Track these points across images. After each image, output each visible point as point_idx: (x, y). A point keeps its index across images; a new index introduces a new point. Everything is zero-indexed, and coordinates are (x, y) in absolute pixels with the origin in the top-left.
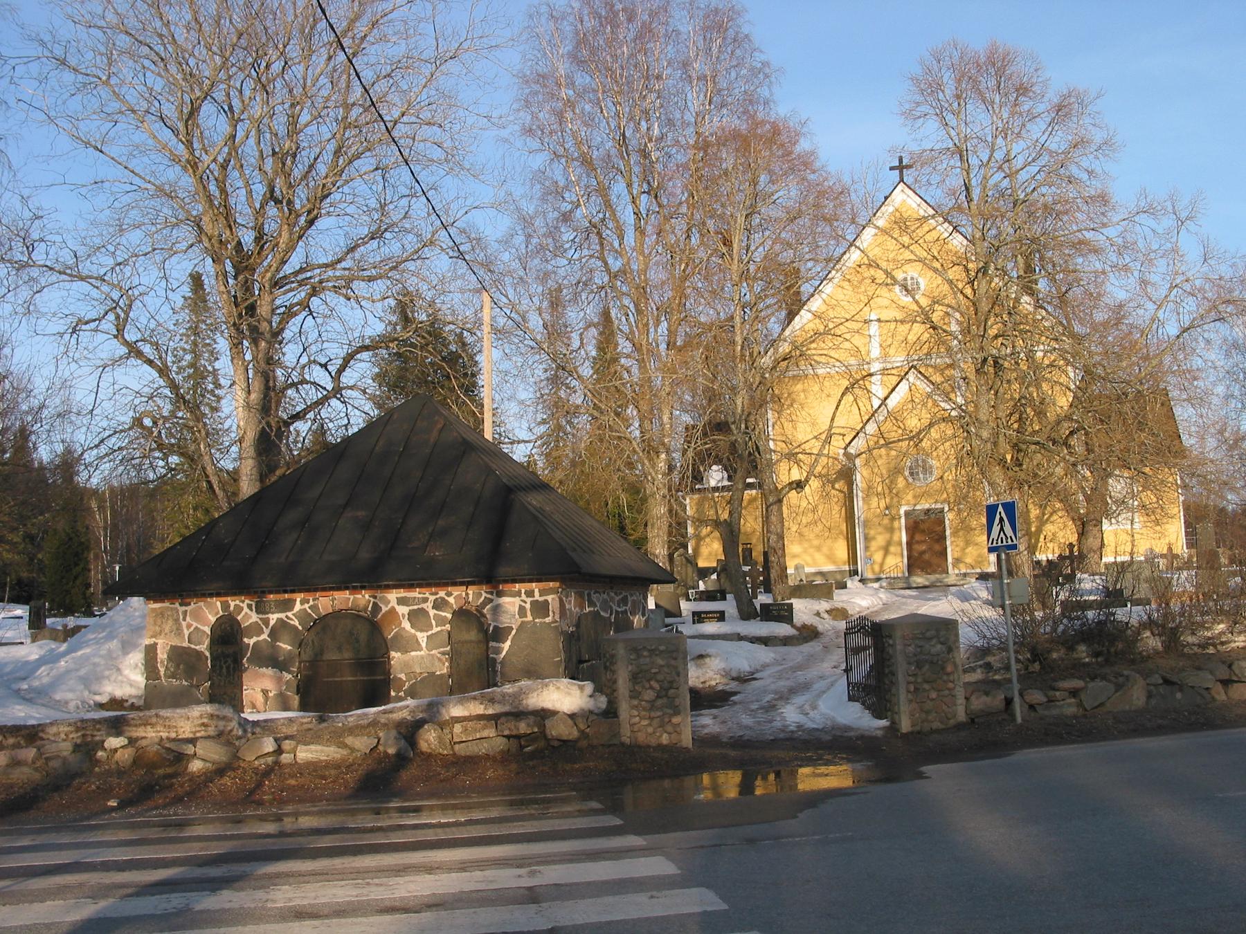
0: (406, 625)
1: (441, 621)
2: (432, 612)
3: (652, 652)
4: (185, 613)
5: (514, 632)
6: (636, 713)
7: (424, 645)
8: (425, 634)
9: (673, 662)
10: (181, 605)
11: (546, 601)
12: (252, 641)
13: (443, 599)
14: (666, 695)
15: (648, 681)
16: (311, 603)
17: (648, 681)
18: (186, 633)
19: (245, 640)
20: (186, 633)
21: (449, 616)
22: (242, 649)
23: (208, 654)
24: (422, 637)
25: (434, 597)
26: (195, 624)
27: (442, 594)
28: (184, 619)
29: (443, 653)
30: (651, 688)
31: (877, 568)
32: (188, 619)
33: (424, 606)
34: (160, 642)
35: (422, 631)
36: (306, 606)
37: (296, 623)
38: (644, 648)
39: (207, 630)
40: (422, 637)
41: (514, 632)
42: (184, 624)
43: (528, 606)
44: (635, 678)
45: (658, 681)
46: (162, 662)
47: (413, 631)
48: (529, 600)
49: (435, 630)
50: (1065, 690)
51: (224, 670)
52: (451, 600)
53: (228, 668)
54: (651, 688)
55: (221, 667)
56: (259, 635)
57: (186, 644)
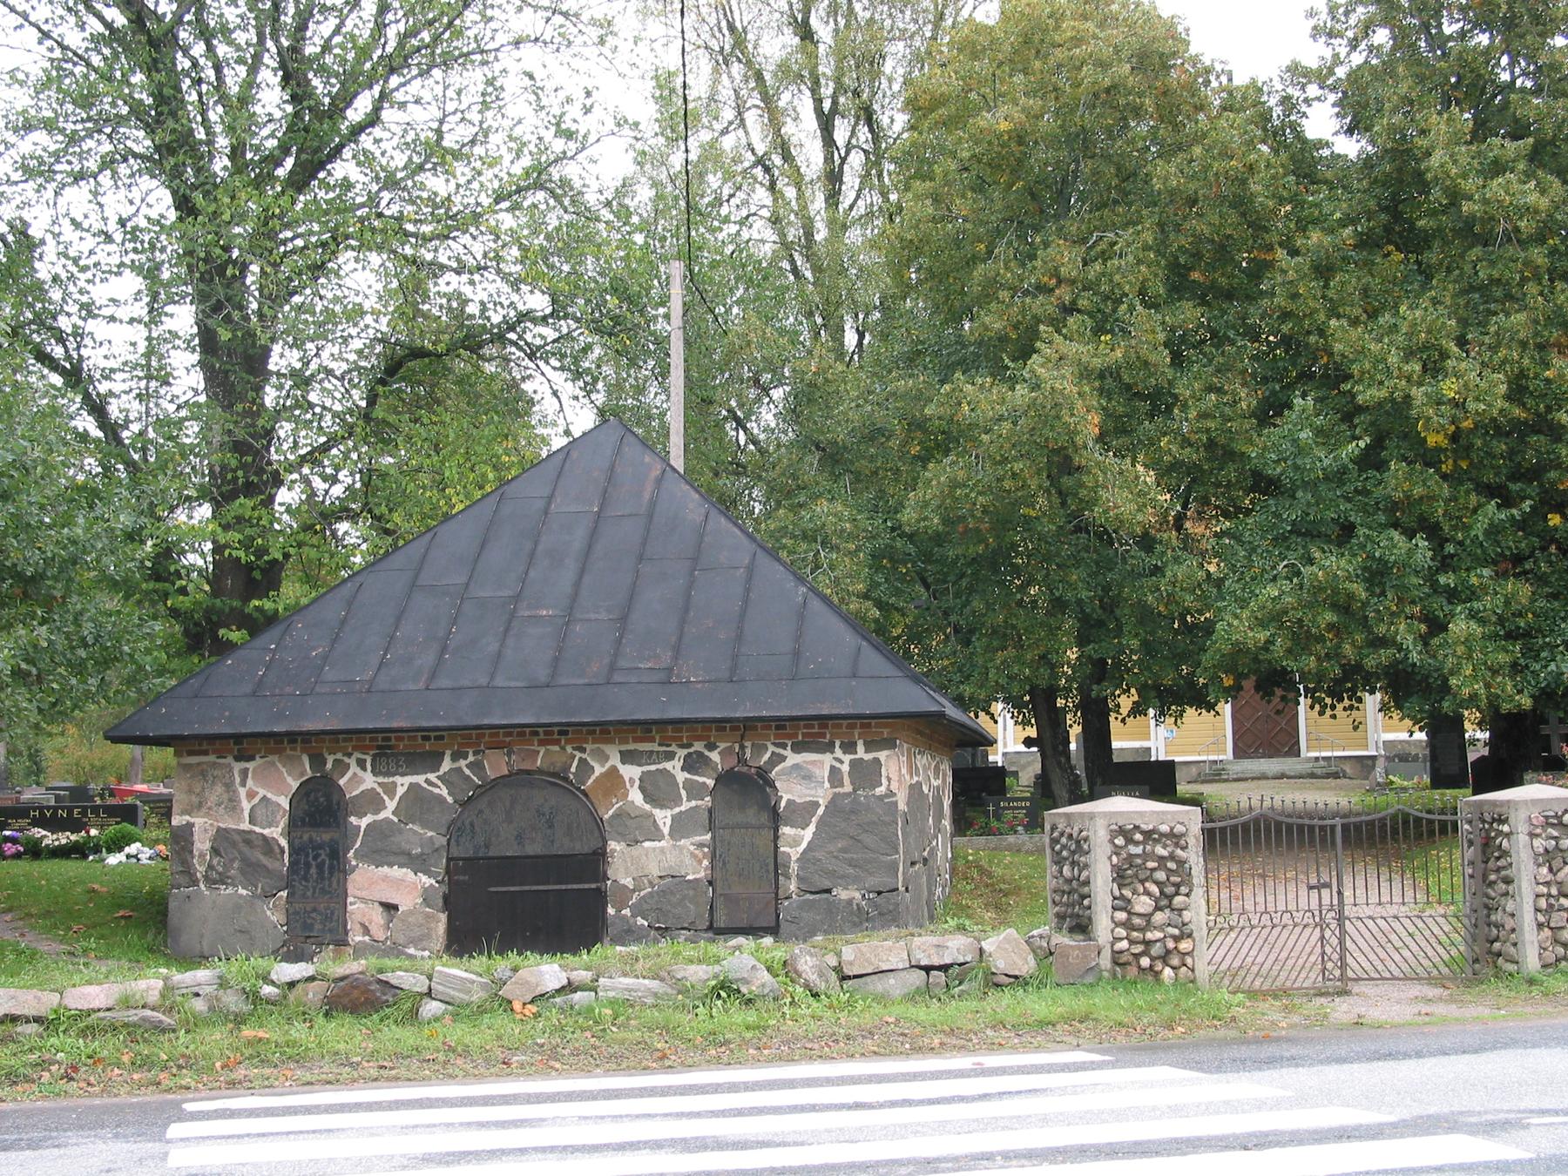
0: (636, 796)
1: (694, 791)
2: (681, 776)
3: (1148, 835)
4: (244, 773)
5: (820, 811)
6: (1124, 933)
7: (666, 831)
8: (669, 813)
9: (1179, 852)
10: (238, 759)
11: (877, 760)
12: (364, 822)
13: (700, 754)
14: (1170, 906)
15: (1142, 882)
16: (471, 758)
17: (1142, 882)
18: (246, 806)
19: (353, 819)
20: (246, 806)
21: (711, 783)
22: (349, 834)
23: (284, 843)
24: (664, 817)
25: (686, 751)
26: (262, 792)
27: (698, 746)
28: (243, 784)
29: (701, 845)
30: (1147, 893)
31: (109, 255)
32: (250, 782)
33: (668, 765)
34: (199, 821)
35: (662, 807)
36: (463, 763)
37: (444, 792)
38: (1136, 828)
39: (284, 802)
40: (664, 817)
41: (820, 811)
42: (242, 792)
43: (845, 768)
44: (1120, 877)
45: (1157, 883)
46: (202, 855)
47: (647, 807)
48: (847, 758)
49: (686, 806)
50: (716, 81)
51: (313, 871)
52: (715, 756)
53: (320, 867)
54: (1147, 893)
55: (308, 865)
56: (377, 812)
57: (245, 826)
